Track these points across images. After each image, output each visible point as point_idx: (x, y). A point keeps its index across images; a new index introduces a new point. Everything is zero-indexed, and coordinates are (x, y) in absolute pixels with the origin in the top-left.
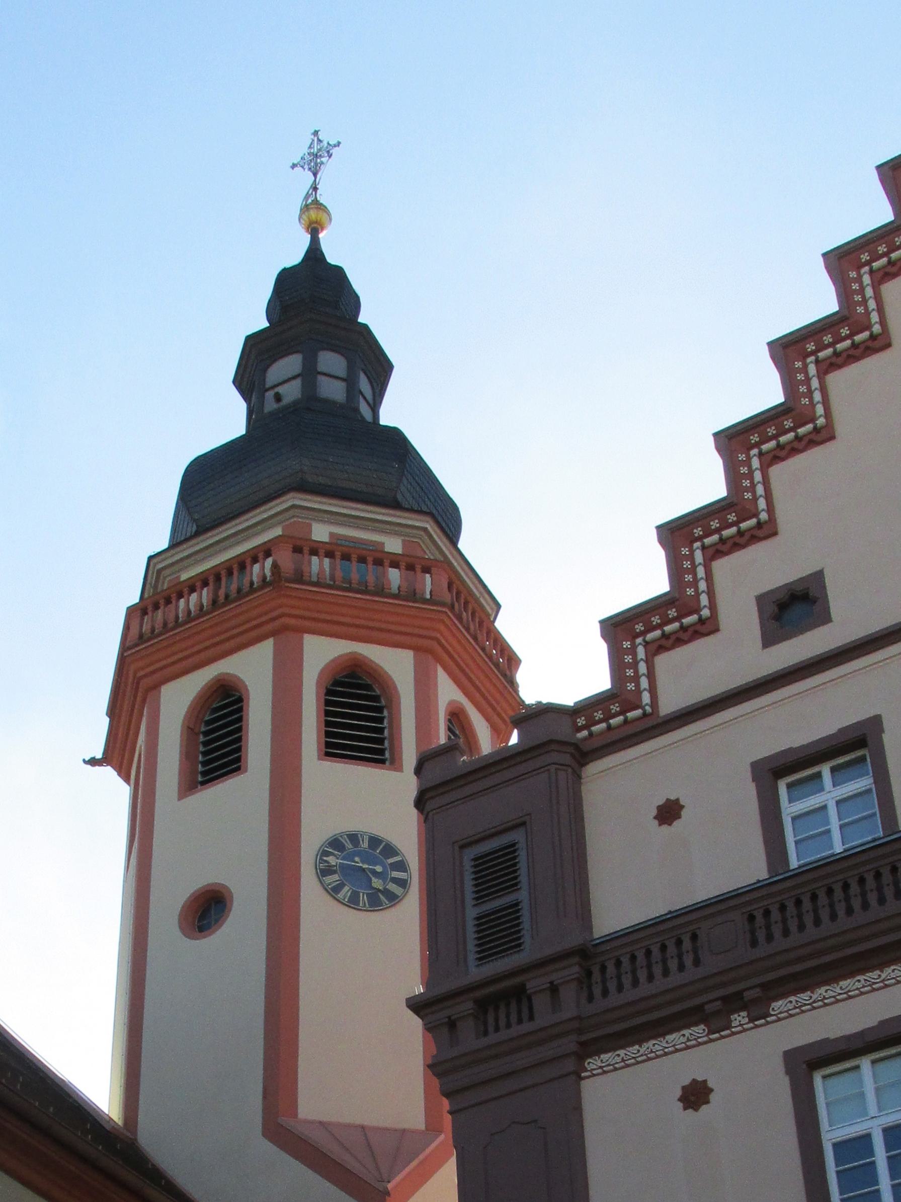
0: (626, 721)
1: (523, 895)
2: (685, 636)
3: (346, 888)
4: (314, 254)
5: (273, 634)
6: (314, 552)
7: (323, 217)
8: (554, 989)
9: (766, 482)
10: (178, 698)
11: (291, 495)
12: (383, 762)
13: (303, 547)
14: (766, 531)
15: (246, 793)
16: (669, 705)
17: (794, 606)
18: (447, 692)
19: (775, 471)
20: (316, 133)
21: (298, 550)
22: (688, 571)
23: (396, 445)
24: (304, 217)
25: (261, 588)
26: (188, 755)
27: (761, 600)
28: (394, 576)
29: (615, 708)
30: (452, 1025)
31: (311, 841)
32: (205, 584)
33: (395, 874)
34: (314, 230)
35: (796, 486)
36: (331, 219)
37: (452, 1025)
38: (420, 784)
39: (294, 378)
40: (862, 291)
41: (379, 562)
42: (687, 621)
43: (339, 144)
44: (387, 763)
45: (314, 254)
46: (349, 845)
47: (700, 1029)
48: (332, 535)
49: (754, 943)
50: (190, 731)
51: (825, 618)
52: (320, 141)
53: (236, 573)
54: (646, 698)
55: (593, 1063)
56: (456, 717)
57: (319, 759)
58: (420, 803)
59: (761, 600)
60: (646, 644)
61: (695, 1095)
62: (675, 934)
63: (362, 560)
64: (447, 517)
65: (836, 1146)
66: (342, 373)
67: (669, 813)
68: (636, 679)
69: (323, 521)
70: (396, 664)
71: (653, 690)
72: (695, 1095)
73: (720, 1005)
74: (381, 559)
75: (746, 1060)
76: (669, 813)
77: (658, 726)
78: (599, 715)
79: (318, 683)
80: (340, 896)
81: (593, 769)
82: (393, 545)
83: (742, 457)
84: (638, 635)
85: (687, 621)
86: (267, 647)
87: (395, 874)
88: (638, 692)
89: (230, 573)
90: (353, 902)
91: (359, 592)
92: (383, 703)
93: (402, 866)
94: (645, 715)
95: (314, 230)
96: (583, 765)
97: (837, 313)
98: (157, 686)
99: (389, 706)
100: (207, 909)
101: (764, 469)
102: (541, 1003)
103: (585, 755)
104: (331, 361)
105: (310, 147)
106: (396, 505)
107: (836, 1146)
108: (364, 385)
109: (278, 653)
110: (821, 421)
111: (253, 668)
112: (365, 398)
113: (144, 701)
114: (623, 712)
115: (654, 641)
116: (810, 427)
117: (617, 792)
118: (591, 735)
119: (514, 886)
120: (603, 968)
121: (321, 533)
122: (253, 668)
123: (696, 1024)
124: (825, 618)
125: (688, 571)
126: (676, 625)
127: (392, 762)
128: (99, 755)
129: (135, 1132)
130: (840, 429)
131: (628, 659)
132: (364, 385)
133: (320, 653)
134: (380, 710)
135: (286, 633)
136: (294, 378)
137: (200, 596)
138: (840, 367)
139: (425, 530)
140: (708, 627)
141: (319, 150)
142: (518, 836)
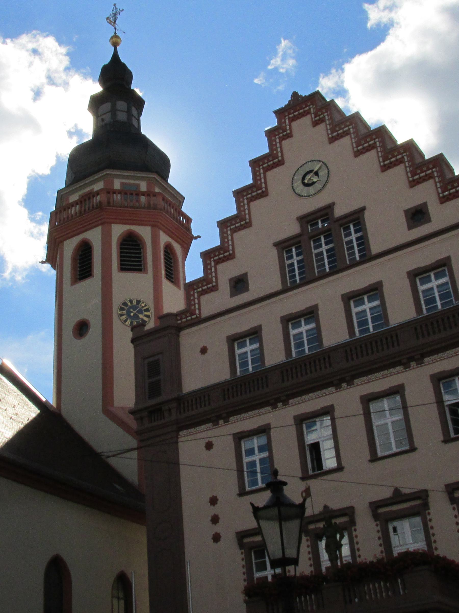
0: (192, 319)
2: (208, 291)
3: (128, 321)
4: (115, 58)
5: (102, 224)
6: (114, 193)
7: (119, 40)
8: (170, 410)
9: (232, 240)
10: (70, 246)
11: (106, 170)
13: (110, 191)
14: (231, 257)
15: (94, 283)
16: (205, 314)
17: (239, 284)
18: (164, 238)
19: (252, 204)
20: (115, 5)
21: (108, 192)
22: (258, 176)
24: (111, 41)
25: (96, 209)
26: (74, 268)
27: (230, 280)
29: (270, 159)
30: (141, 419)
31: (117, 302)
32: (77, 204)
33: (146, 313)
34: (115, 45)
35: (241, 239)
36: (120, 39)
37: (141, 419)
38: (133, 334)
39: (108, 112)
40: (260, 176)
41: (137, 195)
42: (209, 286)
43: (123, 10)
44: (143, 270)
45: (115, 58)
46: (129, 304)
47: (210, 425)
48: (122, 184)
49: (225, 400)
50: (74, 259)
52: (116, 8)
53: (87, 200)
54: (197, 312)
55: (181, 433)
56: (169, 250)
57: (118, 271)
58: (133, 341)
59: (230, 280)
60: (263, 168)
62: (203, 394)
63: (132, 194)
65: (247, 463)
66: (126, 110)
67: (204, 351)
69: (117, 178)
70: (144, 232)
71: (199, 309)
73: (217, 417)
75: (221, 435)
76: (204, 351)
77: (201, 321)
78: (217, 253)
79: (118, 240)
80: (127, 323)
81: (184, 333)
83: (208, 262)
84: (212, 258)
85: (209, 286)
86: (99, 229)
87: (146, 313)
88: (195, 309)
89: (85, 200)
91: (130, 207)
92: (141, 247)
94: (197, 317)
95: (115, 45)
96: (180, 332)
97: (251, 184)
98: (62, 242)
99: (143, 248)
100: (82, 328)
101: (280, 143)
103: (180, 329)
104: (121, 105)
105: (113, 11)
107: (247, 463)
108: (134, 111)
109: (103, 230)
110: (248, 221)
111: (94, 236)
112: (135, 117)
114: (206, 285)
115: (266, 167)
116: (244, 222)
117: (190, 340)
118: (182, 322)
120: (184, 404)
122: (94, 236)
123: (210, 423)
125: (258, 176)
126: (272, 162)
127: (144, 271)
128: (44, 260)
129: (60, 411)
130: (254, 222)
131: (226, 235)
133: (118, 230)
134: (140, 249)
135: (105, 224)
136: (108, 112)
137: (76, 208)
138: (270, 170)
139: (155, 178)
140: (215, 288)
141: (116, 12)
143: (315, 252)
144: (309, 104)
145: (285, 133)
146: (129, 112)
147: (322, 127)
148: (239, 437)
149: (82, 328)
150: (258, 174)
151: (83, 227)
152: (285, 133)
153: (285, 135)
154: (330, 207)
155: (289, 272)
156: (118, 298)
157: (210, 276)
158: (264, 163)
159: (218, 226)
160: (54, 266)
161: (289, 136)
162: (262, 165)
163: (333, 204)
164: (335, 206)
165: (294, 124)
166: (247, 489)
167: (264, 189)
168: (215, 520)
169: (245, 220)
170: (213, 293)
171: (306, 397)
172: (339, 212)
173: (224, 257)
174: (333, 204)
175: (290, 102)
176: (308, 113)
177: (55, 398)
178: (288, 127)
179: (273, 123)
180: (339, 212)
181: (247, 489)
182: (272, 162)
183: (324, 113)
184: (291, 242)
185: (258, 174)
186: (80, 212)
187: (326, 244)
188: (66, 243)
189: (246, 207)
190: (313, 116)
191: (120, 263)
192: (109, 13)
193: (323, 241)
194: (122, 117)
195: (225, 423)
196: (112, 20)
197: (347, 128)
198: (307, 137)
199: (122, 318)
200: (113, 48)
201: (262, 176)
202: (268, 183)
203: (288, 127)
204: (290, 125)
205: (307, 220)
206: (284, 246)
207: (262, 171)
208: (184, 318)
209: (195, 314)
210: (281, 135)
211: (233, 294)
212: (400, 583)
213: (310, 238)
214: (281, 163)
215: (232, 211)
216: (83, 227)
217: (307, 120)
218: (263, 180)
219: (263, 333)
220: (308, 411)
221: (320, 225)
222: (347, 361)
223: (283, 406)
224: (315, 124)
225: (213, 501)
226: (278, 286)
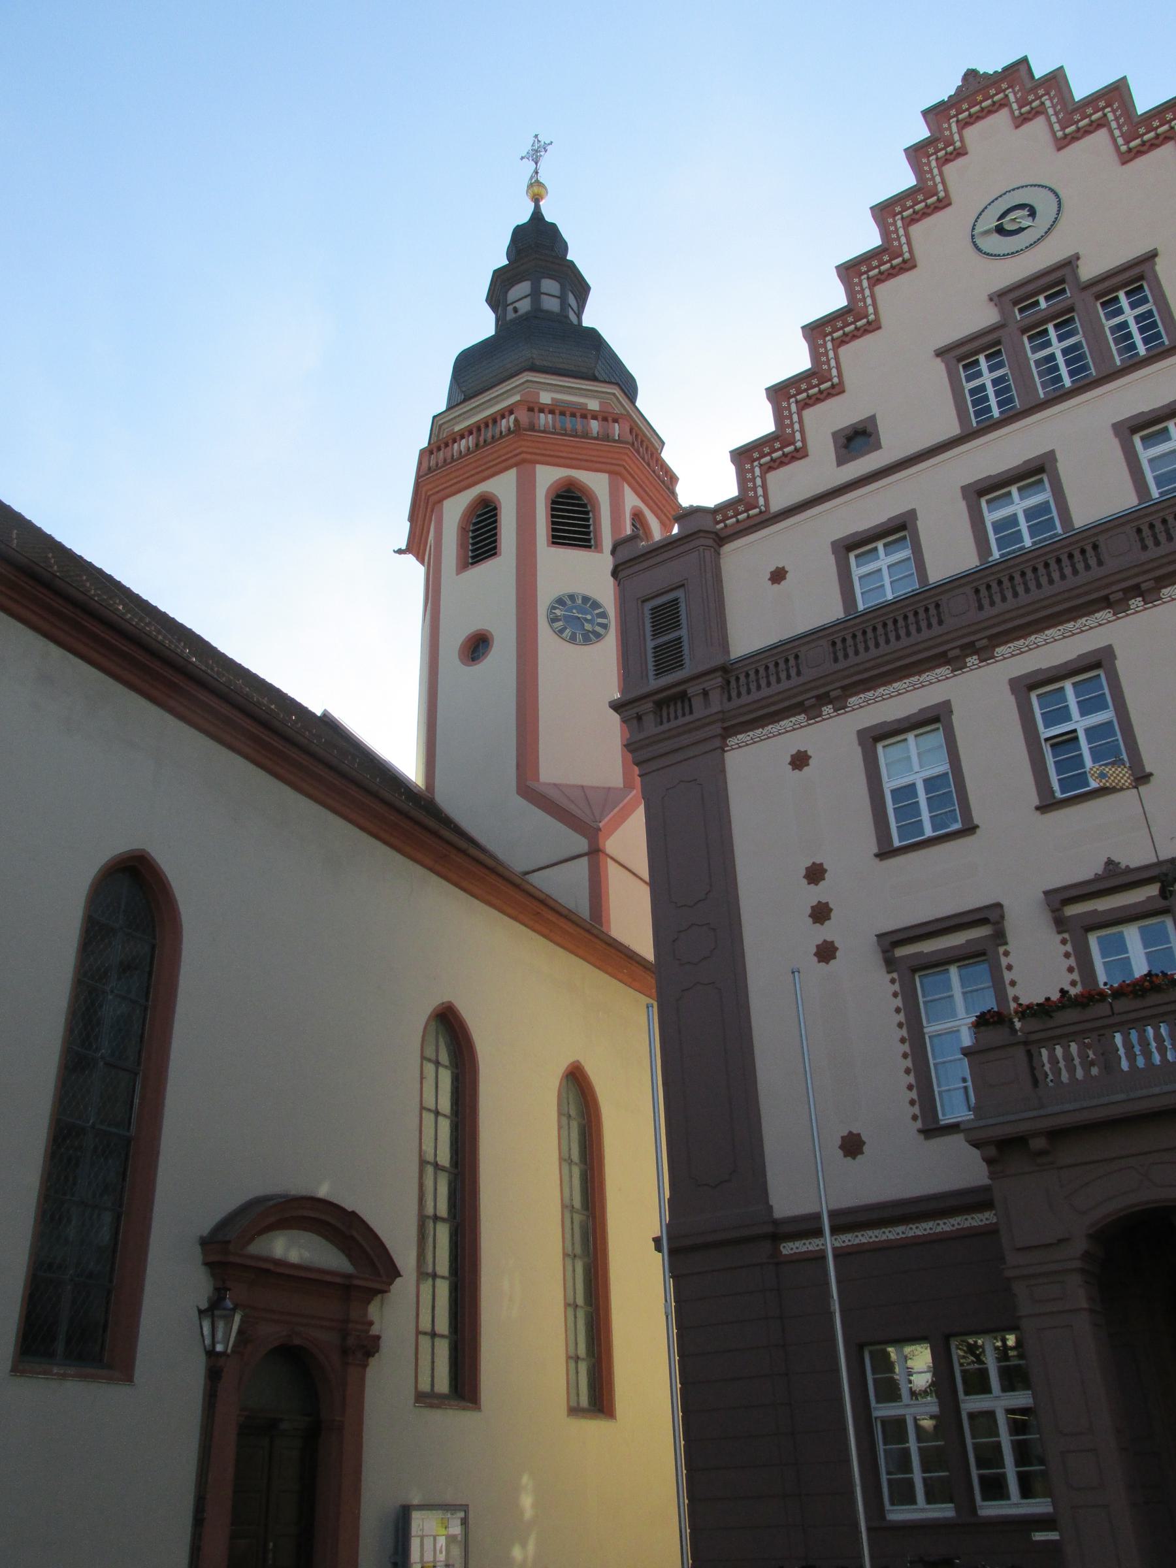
0: (748, 517)
1: (683, 632)
2: (786, 460)
4: (537, 216)
5: (516, 465)
6: (541, 411)
7: (543, 191)
8: (705, 693)
10: (455, 509)
12: (590, 547)
13: (534, 408)
14: (837, 390)
15: (500, 570)
16: (776, 506)
17: (857, 438)
18: (631, 500)
20: (536, 136)
21: (531, 409)
23: (593, 339)
26: (462, 545)
28: (595, 425)
30: (639, 718)
32: (471, 433)
33: (600, 620)
34: (536, 200)
37: (639, 718)
45: (537, 216)
46: (569, 602)
48: (553, 399)
50: (463, 530)
51: (877, 446)
54: (761, 501)
55: (732, 741)
56: (637, 517)
58: (615, 574)
61: (800, 761)
62: (784, 655)
63: (573, 415)
64: (628, 386)
67: (778, 576)
68: (755, 489)
70: (597, 483)
71: (766, 496)
72: (800, 761)
74: (586, 415)
75: (833, 736)
76: (778, 576)
80: (564, 635)
81: (727, 548)
82: (593, 405)
84: (755, 460)
86: (512, 474)
87: (600, 620)
88: (756, 497)
90: (572, 639)
91: (571, 436)
92: (589, 508)
93: (604, 615)
94: (761, 512)
95: (536, 200)
96: (721, 546)
98: (441, 501)
100: (477, 646)
101: (940, 168)
102: (697, 702)
103: (721, 539)
104: (549, 286)
106: (595, 379)
108: (572, 300)
111: (503, 487)
113: (432, 511)
116: (864, 321)
117: (743, 563)
119: (677, 626)
121: (546, 398)
122: (503, 487)
123: (799, 714)
124: (877, 446)
128: (404, 547)
129: (433, 792)
132: (572, 300)
133: (547, 477)
134: (587, 513)
135: (525, 464)
140: (800, 454)
142: (679, 593)
143: (1033, 357)
144: (1004, 86)
145: (950, 149)
146: (563, 299)
147: (1038, 126)
148: (874, 738)
149: (477, 646)
150: (786, 413)
151: (478, 473)
152: (950, 149)
153: (951, 153)
154: (1070, 263)
155: (975, 403)
156: (546, 593)
157: (896, 243)
158: (871, 269)
159: (769, 399)
160: (421, 559)
161: (961, 153)
162: (794, 396)
163: (1077, 257)
164: (1079, 262)
165: (969, 132)
166: (897, 843)
167: (836, 380)
168: (821, 913)
169: (866, 316)
170: (869, 338)
171: (1038, 638)
172: (1087, 271)
173: (785, 455)
174: (1077, 257)
175: (959, 89)
176: (1004, 103)
177: (422, 768)
178: (956, 137)
179: (921, 132)
180: (1087, 271)
181: (897, 843)
182: (780, 453)
183: (1043, 96)
184: (976, 344)
185: (786, 413)
186: (477, 445)
187: (1061, 338)
188: (447, 504)
189: (759, 482)
190: (1015, 106)
191: (550, 519)
192: (526, 147)
193: (1053, 334)
194: (551, 305)
195: (835, 711)
196: (536, 154)
197: (1100, 114)
198: (1003, 153)
199: (556, 625)
200: (533, 204)
201: (759, 482)
202: (914, 243)
203: (956, 137)
204: (941, 174)
205: (1016, 297)
206: (961, 355)
207: (829, 345)
208: (732, 517)
209: (830, 380)
210: (941, 154)
211: (841, 461)
212: (1154, 1050)
213: (1024, 331)
214: (943, 204)
215: (907, 180)
216: (478, 473)
217: (1002, 118)
218: (760, 491)
219: (920, 524)
220: (1045, 665)
221: (1043, 304)
222: (1145, 548)
223: (981, 661)
224: (1021, 121)
225: (815, 874)
226: (953, 429)
